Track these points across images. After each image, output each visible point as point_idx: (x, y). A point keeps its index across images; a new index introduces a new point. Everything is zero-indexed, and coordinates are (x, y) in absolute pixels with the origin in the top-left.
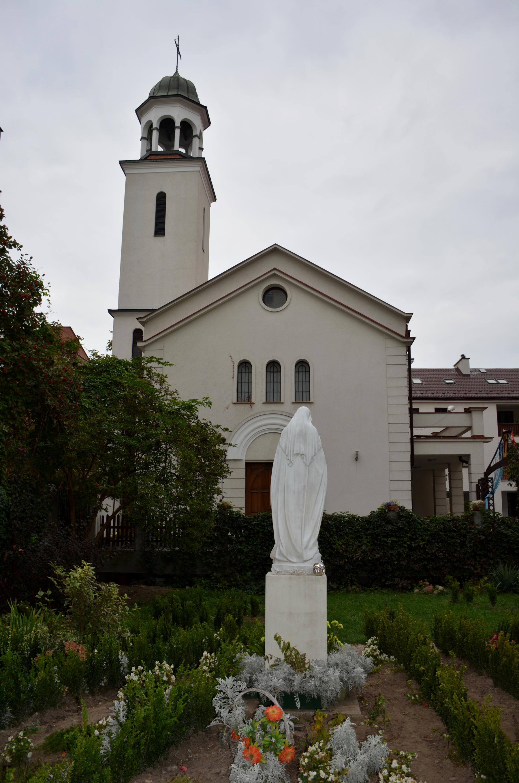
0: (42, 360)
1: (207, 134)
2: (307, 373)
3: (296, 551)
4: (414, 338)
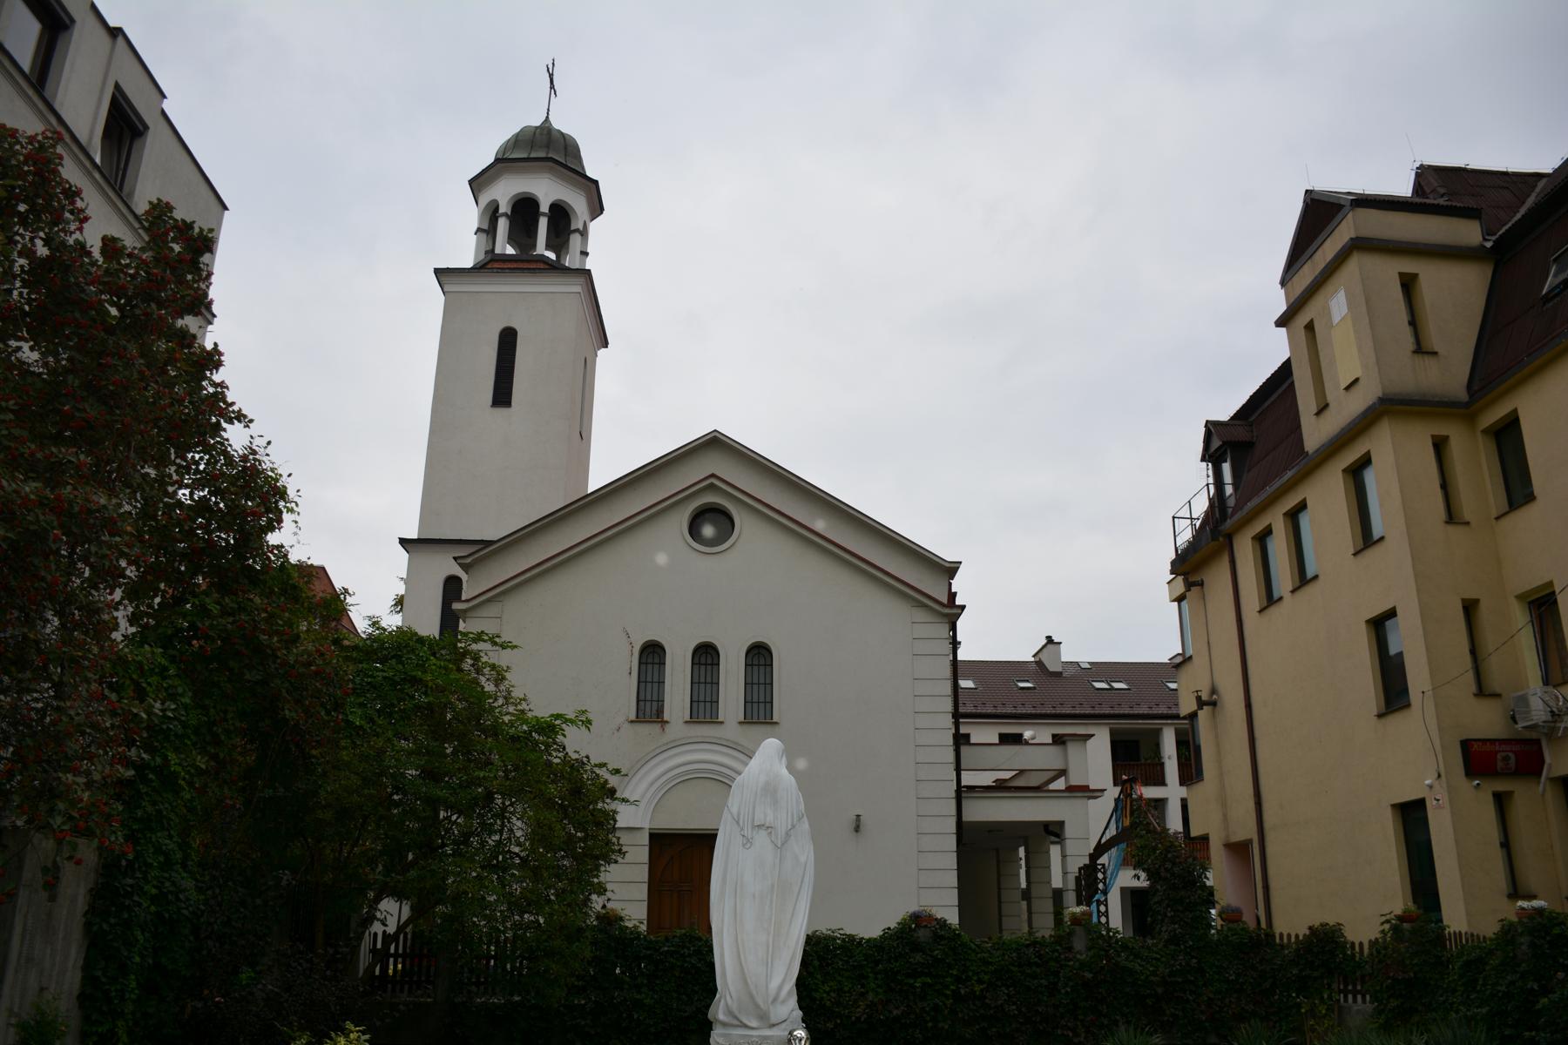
0: (277, 633)
1: (595, 227)
3: (757, 1006)
4: (963, 607)
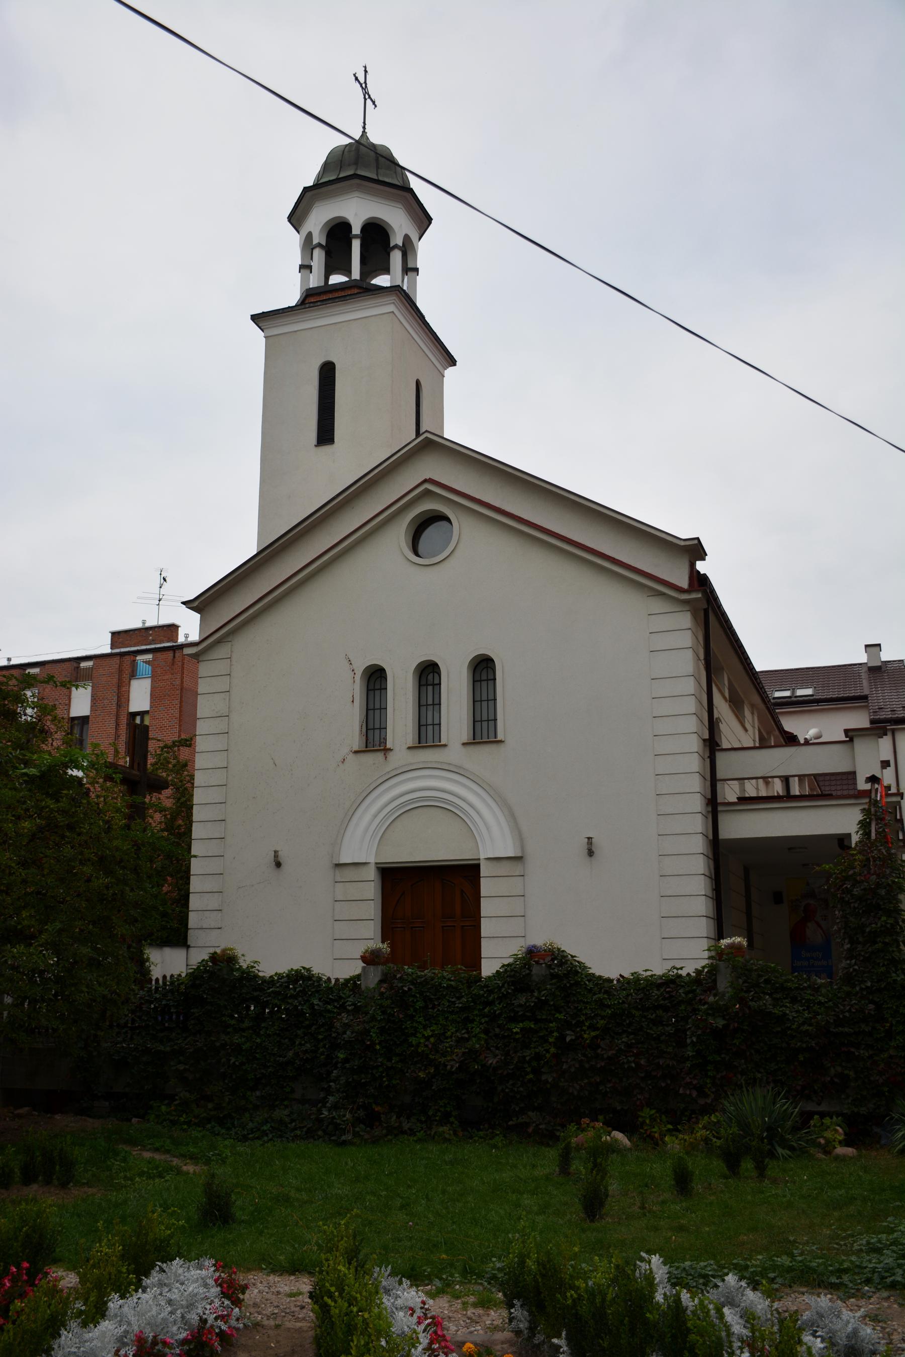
2: (491, 683)
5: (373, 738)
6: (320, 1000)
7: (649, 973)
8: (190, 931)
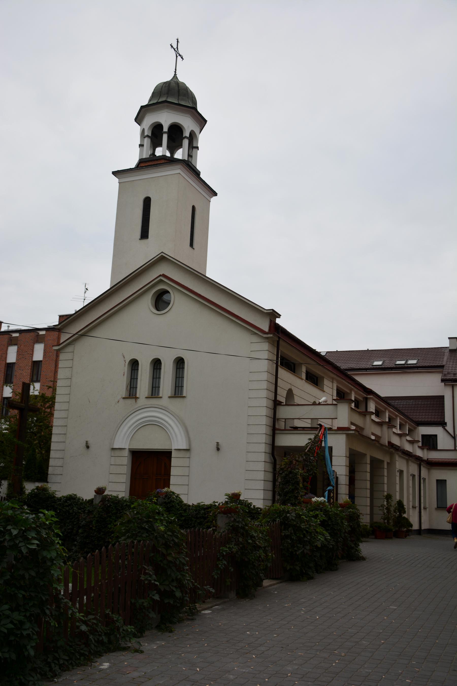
5: (132, 393)
6: (77, 508)
7: (203, 504)
8: (49, 476)
